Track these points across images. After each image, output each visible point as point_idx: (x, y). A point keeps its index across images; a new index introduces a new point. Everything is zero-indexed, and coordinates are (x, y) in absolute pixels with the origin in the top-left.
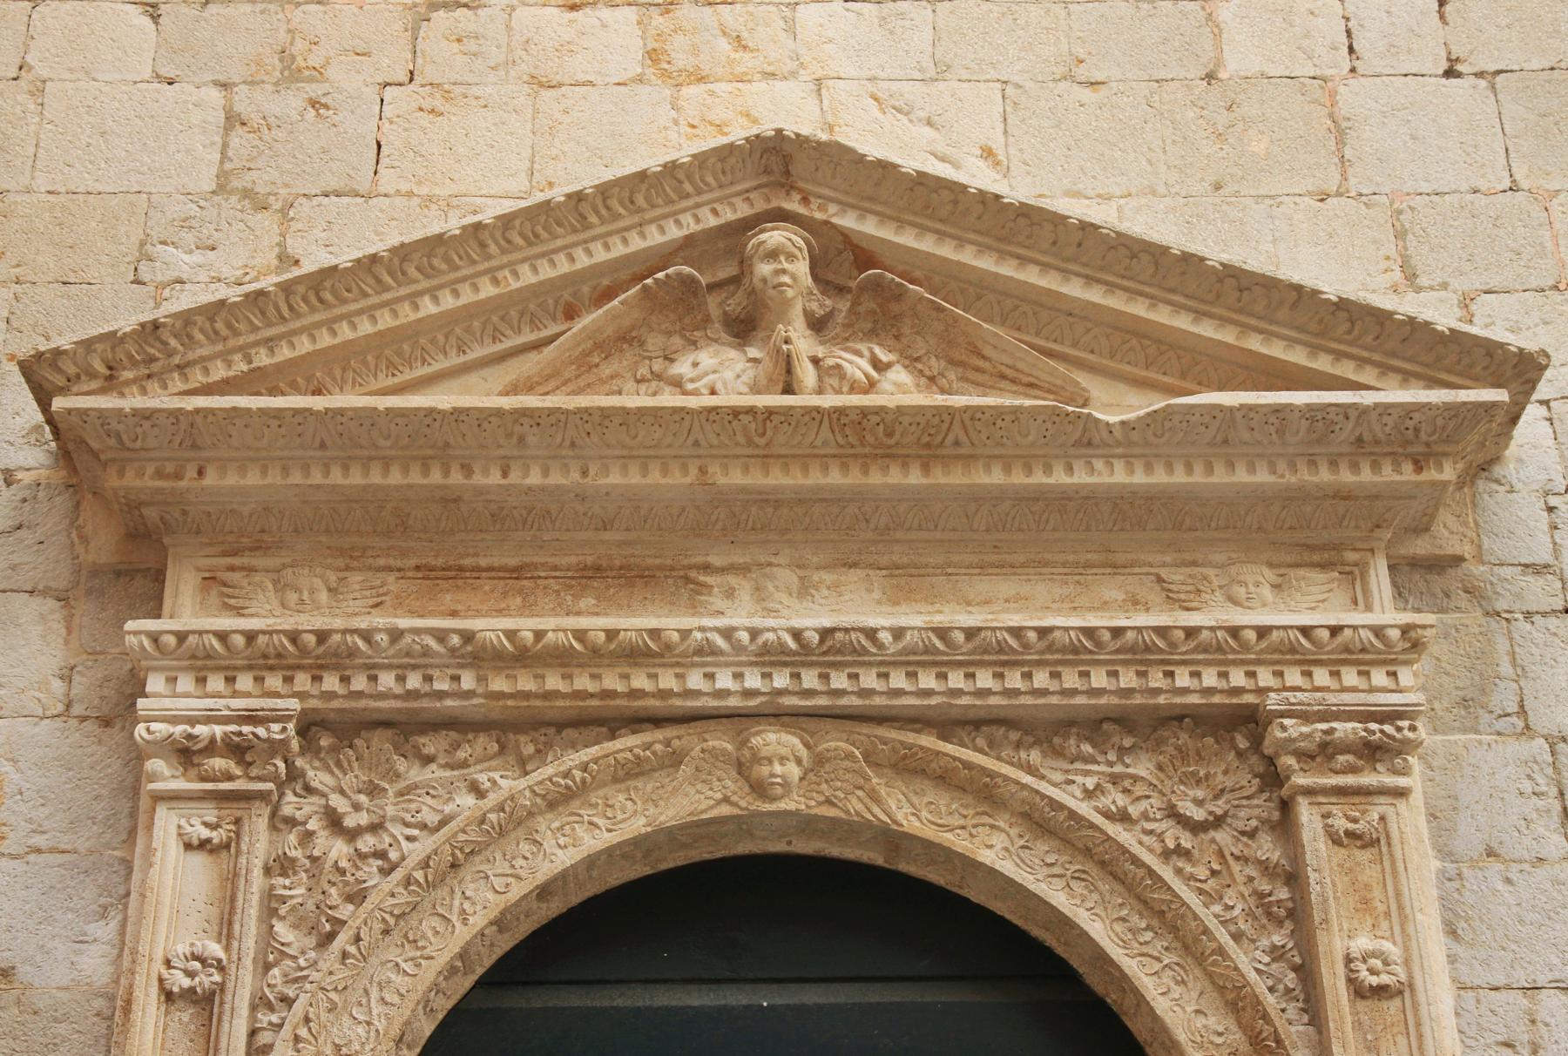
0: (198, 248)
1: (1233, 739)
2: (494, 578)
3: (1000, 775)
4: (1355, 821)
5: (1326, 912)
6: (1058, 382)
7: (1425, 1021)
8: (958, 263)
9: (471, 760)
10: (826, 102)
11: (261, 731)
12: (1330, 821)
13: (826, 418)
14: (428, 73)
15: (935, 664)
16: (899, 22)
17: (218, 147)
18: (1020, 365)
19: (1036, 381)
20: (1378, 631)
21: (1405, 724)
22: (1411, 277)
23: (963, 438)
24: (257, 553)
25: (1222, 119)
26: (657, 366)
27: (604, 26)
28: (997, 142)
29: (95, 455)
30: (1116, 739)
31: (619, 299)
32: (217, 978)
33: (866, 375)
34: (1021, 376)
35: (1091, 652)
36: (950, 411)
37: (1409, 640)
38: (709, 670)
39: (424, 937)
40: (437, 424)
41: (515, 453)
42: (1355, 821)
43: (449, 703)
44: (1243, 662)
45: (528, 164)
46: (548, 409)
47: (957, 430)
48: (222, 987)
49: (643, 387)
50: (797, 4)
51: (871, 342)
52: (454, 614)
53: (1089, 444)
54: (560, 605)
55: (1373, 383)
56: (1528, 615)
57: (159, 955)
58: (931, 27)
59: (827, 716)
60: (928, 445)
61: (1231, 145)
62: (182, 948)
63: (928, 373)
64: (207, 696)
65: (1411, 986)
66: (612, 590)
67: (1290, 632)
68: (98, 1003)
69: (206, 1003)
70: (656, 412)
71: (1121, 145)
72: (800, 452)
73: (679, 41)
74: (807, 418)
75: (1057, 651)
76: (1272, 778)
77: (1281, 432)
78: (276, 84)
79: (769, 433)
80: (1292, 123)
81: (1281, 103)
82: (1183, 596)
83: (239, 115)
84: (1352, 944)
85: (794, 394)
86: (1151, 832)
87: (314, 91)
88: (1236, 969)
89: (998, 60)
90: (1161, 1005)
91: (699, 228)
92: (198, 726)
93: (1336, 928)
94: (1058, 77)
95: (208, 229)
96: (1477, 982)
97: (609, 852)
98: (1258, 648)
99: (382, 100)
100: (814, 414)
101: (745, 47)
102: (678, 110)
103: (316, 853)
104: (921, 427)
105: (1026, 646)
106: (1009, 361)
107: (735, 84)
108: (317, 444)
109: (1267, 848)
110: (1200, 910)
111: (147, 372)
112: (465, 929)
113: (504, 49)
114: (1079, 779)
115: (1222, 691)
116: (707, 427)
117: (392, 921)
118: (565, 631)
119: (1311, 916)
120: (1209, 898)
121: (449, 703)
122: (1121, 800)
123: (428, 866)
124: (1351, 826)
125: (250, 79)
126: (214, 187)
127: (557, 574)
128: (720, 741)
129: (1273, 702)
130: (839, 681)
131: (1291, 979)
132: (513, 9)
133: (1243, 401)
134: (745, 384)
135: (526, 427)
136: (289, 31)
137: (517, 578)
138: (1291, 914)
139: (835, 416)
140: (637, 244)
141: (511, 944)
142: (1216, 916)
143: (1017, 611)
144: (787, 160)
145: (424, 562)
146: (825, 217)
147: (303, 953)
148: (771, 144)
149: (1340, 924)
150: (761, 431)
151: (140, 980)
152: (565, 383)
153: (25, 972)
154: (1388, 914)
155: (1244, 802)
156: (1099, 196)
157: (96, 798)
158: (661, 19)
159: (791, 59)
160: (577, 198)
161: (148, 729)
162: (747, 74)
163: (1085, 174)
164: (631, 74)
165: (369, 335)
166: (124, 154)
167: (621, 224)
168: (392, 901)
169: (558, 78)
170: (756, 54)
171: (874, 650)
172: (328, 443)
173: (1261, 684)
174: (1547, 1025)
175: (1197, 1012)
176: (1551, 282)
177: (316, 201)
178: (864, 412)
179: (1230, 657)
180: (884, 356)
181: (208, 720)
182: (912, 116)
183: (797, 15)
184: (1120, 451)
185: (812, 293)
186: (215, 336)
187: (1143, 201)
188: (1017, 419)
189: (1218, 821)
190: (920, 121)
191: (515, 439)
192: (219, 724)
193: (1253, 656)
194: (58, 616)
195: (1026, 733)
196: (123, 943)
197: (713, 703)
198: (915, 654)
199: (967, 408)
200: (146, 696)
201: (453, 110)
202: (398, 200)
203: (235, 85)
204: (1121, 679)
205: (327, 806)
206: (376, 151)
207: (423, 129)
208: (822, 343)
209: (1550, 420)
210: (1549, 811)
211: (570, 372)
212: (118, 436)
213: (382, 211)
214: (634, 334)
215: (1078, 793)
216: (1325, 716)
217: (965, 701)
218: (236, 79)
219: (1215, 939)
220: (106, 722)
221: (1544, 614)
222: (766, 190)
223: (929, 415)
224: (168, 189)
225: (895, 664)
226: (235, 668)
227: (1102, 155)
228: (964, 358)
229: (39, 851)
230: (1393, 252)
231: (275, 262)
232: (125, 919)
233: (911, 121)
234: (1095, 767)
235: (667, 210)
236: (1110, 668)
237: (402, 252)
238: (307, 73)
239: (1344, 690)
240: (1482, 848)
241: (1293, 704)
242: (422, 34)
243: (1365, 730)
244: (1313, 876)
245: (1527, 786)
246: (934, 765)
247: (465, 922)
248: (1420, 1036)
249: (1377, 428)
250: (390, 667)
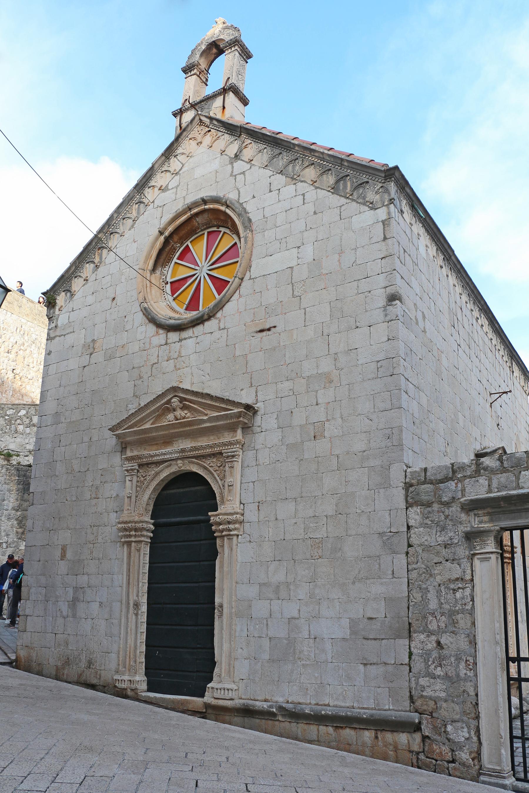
128: (174, 462)
186: (125, 422)
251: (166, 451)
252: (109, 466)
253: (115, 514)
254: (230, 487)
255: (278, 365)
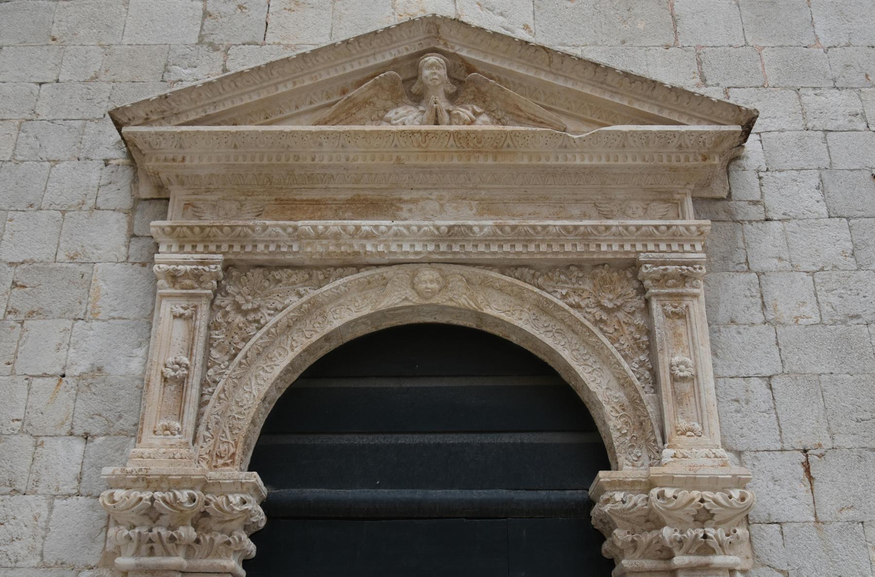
1: (625, 273)
3: (525, 288)
4: (676, 307)
5: (662, 346)
6: (554, 121)
7: (702, 390)
8: (511, 70)
9: (297, 282)
10: (458, 6)
11: (206, 268)
12: (665, 307)
17: (200, 25)
18: (537, 114)
20: (687, 228)
21: (697, 266)
22: (704, 81)
23: (511, 144)
25: (626, 14)
26: (381, 114)
28: (530, 22)
29: (140, 151)
30: (576, 273)
32: (186, 372)
35: (565, 236)
36: (506, 133)
37: (700, 231)
38: (400, 243)
39: (275, 356)
42: (676, 307)
43: (288, 257)
47: (509, 141)
48: (188, 376)
49: (374, 122)
52: (291, 220)
54: (337, 215)
55: (686, 123)
56: (750, 222)
57: (161, 362)
60: (496, 147)
62: (171, 359)
63: (497, 117)
65: (697, 376)
66: (359, 210)
68: (137, 382)
69: (181, 383)
74: (444, 135)
76: (642, 290)
77: (647, 143)
79: (427, 142)
82: (605, 213)
84: (673, 359)
86: (590, 313)
88: (624, 370)
90: (592, 386)
91: (399, 56)
93: (666, 353)
96: (725, 375)
97: (356, 321)
103: (230, 320)
109: (639, 320)
110: (610, 346)
112: (292, 353)
114: (559, 290)
115: (621, 253)
116: (401, 139)
117: (261, 350)
119: (656, 347)
120: (613, 341)
121: (288, 257)
122: (577, 299)
123: (277, 326)
124: (673, 309)
126: (197, 41)
129: (642, 257)
130: (456, 248)
131: (647, 374)
135: (323, 138)
138: (649, 347)
139: (456, 134)
140: (372, 62)
141: (315, 360)
142: (616, 348)
144: (438, 27)
147: (223, 362)
149: (668, 351)
151: (153, 372)
153: (107, 369)
154: (688, 346)
155: (630, 300)
156: (574, 45)
157: (138, 296)
161: (159, 267)
168: (261, 341)
172: (238, 146)
173: (637, 250)
174: (753, 392)
175: (607, 388)
176: (761, 84)
177: (239, 47)
178: (468, 133)
179: (625, 238)
180: (479, 110)
181: (184, 264)
182: (494, 12)
184: (578, 150)
187: (592, 48)
189: (618, 308)
191: (317, 144)
194: (124, 220)
195: (537, 270)
196: (148, 357)
197: (402, 257)
199: (512, 132)
200: (159, 253)
201: (299, 9)
202: (274, 46)
205: (234, 301)
207: (286, 17)
208: (452, 105)
209: (761, 141)
210: (757, 303)
212: (150, 143)
215: (559, 296)
216: (664, 263)
217: (510, 257)
219: (615, 358)
220: (144, 265)
221: (757, 222)
225: (481, 241)
226: (197, 242)
228: (513, 111)
229: (114, 318)
230: (696, 70)
232: (149, 347)
234: (566, 285)
236: (411, 243)
239: (673, 252)
240: (728, 319)
243: (681, 269)
244: (657, 331)
245: (748, 293)
246: (497, 284)
247: (292, 350)
248: (700, 397)
249: (688, 141)
250: (263, 241)
251: (376, 227)
252: (61, 256)
253: (78, 446)
254: (676, 385)
255: (794, 43)
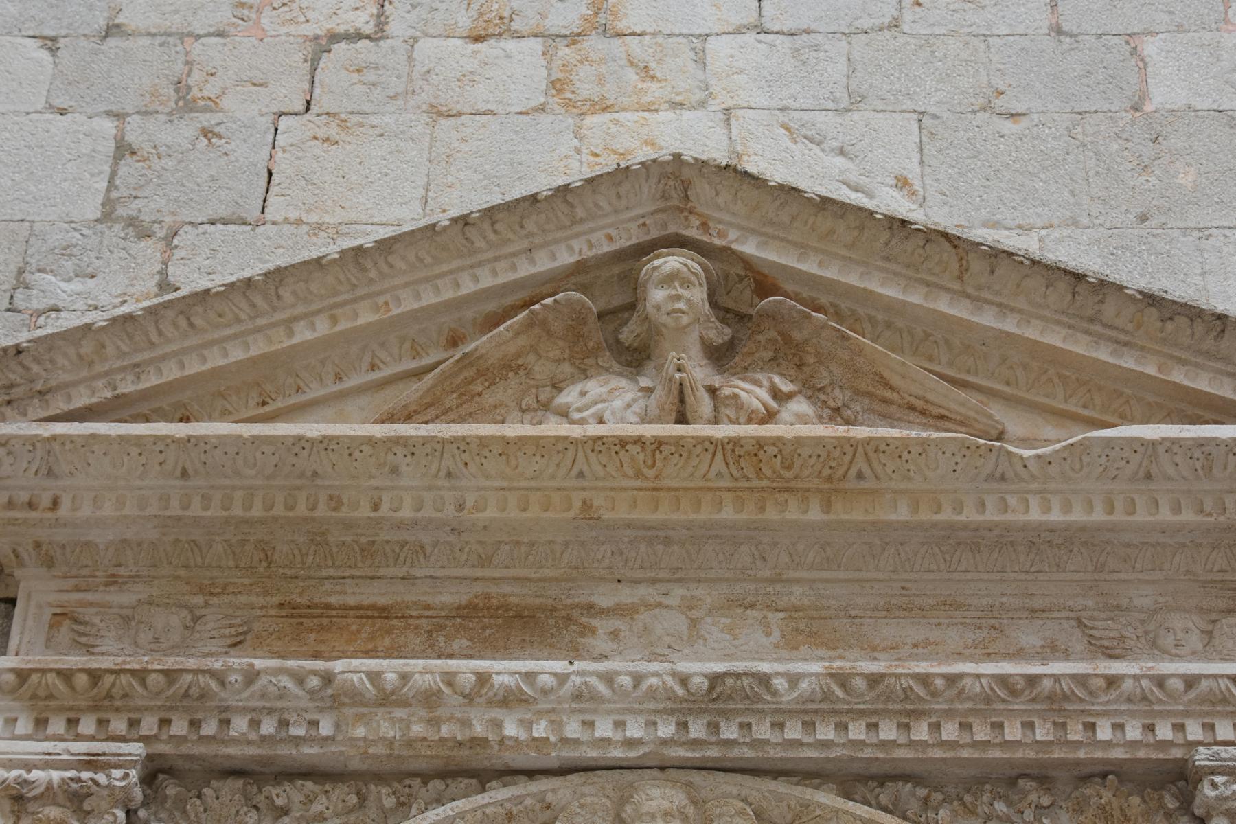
0: (77, 276)
1: (1161, 798)
2: (362, 617)
6: (971, 414)
8: (865, 290)
10: (735, 132)
11: (101, 778)
13: (720, 447)
14: (323, 101)
15: (834, 712)
16: (814, 54)
17: (106, 176)
19: (946, 413)
23: (866, 471)
24: (112, 588)
27: (508, 56)
28: (912, 170)
30: (1033, 797)
31: (505, 325)
33: (764, 405)
34: (931, 408)
35: (1004, 701)
36: (853, 443)
38: (588, 717)
40: (305, 453)
41: (388, 483)
43: (306, 750)
44: (1169, 713)
45: (423, 192)
46: (423, 437)
47: (860, 463)
49: (528, 416)
50: (708, 35)
51: (772, 372)
52: (316, 656)
53: (1003, 478)
54: (431, 646)
58: (845, 59)
59: (673, 767)
60: (830, 479)
61: (1158, 177)
63: (832, 404)
64: (47, 739)
67: (1220, 681)
70: (538, 443)
71: (1043, 176)
72: (691, 485)
73: (585, 71)
74: (699, 449)
75: (969, 699)
78: (170, 114)
79: (659, 464)
80: (1220, 155)
81: (1209, 136)
82: (1105, 643)
83: (130, 145)
85: (687, 423)
87: (209, 121)
89: (915, 92)
92: (34, 772)
94: (976, 108)
95: (89, 257)
98: (1186, 699)
99: (276, 130)
100: (707, 444)
101: (653, 77)
102: (581, 139)
104: (822, 459)
105: (934, 694)
106: (920, 393)
107: (641, 114)
108: (178, 473)
111: (7, 398)
113: (404, 79)
118: (432, 672)
121: (306, 750)
125: (144, 109)
126: (98, 215)
127: (430, 613)
129: (1202, 758)
130: (730, 732)
132: (416, 40)
133: (1164, 435)
134: (635, 413)
136: (187, 63)
137: (386, 618)
139: (729, 447)
140: (525, 270)
143: (925, 658)
144: (686, 186)
145: (288, 599)
146: (724, 243)
148: (669, 169)
150: (650, 462)
152: (445, 413)
156: (1020, 227)
158: (567, 50)
159: (700, 89)
160: (463, 221)
162: (654, 104)
163: (1004, 204)
164: (534, 103)
165: (240, 361)
166: (9, 183)
167: (509, 249)
169: (459, 107)
170: (664, 84)
171: (768, 698)
172: (190, 472)
173: (1190, 738)
177: (201, 229)
178: (760, 443)
179: (1156, 707)
180: (786, 387)
181: (47, 765)
182: (824, 146)
183: (707, 46)
185: (709, 320)
187: (1065, 232)
188: (924, 451)
190: (833, 150)
192: (57, 769)
193: (1181, 708)
197: (593, 753)
198: (813, 701)
199: (869, 440)
203: (128, 115)
204: (1038, 731)
206: (266, 179)
207: (316, 158)
211: (451, 401)
213: (269, 238)
214: (520, 362)
217: (868, 753)
218: (129, 109)
222: (664, 216)
223: (830, 447)
224: (51, 218)
226: (80, 710)
227: (1023, 186)
228: (870, 388)
231: (156, 290)
233: (823, 151)
235: (559, 234)
237: (277, 276)
238: (201, 103)
241: (1225, 760)
242: (321, 65)
250: (244, 710)
